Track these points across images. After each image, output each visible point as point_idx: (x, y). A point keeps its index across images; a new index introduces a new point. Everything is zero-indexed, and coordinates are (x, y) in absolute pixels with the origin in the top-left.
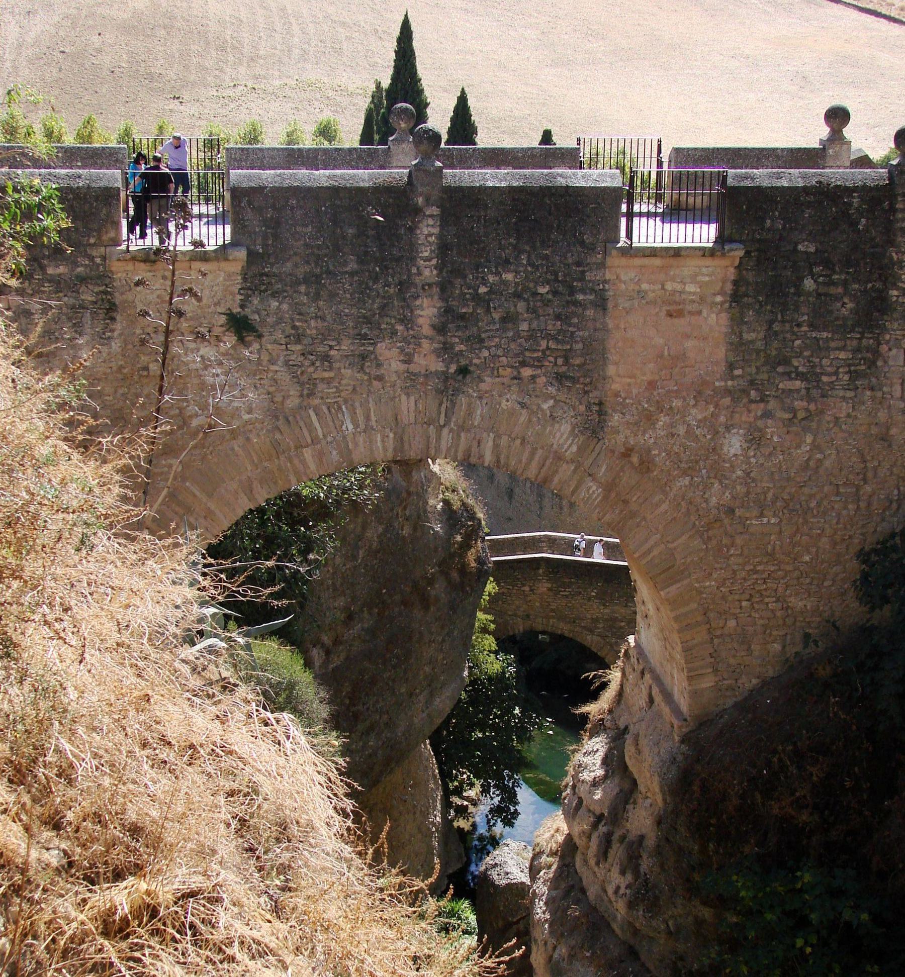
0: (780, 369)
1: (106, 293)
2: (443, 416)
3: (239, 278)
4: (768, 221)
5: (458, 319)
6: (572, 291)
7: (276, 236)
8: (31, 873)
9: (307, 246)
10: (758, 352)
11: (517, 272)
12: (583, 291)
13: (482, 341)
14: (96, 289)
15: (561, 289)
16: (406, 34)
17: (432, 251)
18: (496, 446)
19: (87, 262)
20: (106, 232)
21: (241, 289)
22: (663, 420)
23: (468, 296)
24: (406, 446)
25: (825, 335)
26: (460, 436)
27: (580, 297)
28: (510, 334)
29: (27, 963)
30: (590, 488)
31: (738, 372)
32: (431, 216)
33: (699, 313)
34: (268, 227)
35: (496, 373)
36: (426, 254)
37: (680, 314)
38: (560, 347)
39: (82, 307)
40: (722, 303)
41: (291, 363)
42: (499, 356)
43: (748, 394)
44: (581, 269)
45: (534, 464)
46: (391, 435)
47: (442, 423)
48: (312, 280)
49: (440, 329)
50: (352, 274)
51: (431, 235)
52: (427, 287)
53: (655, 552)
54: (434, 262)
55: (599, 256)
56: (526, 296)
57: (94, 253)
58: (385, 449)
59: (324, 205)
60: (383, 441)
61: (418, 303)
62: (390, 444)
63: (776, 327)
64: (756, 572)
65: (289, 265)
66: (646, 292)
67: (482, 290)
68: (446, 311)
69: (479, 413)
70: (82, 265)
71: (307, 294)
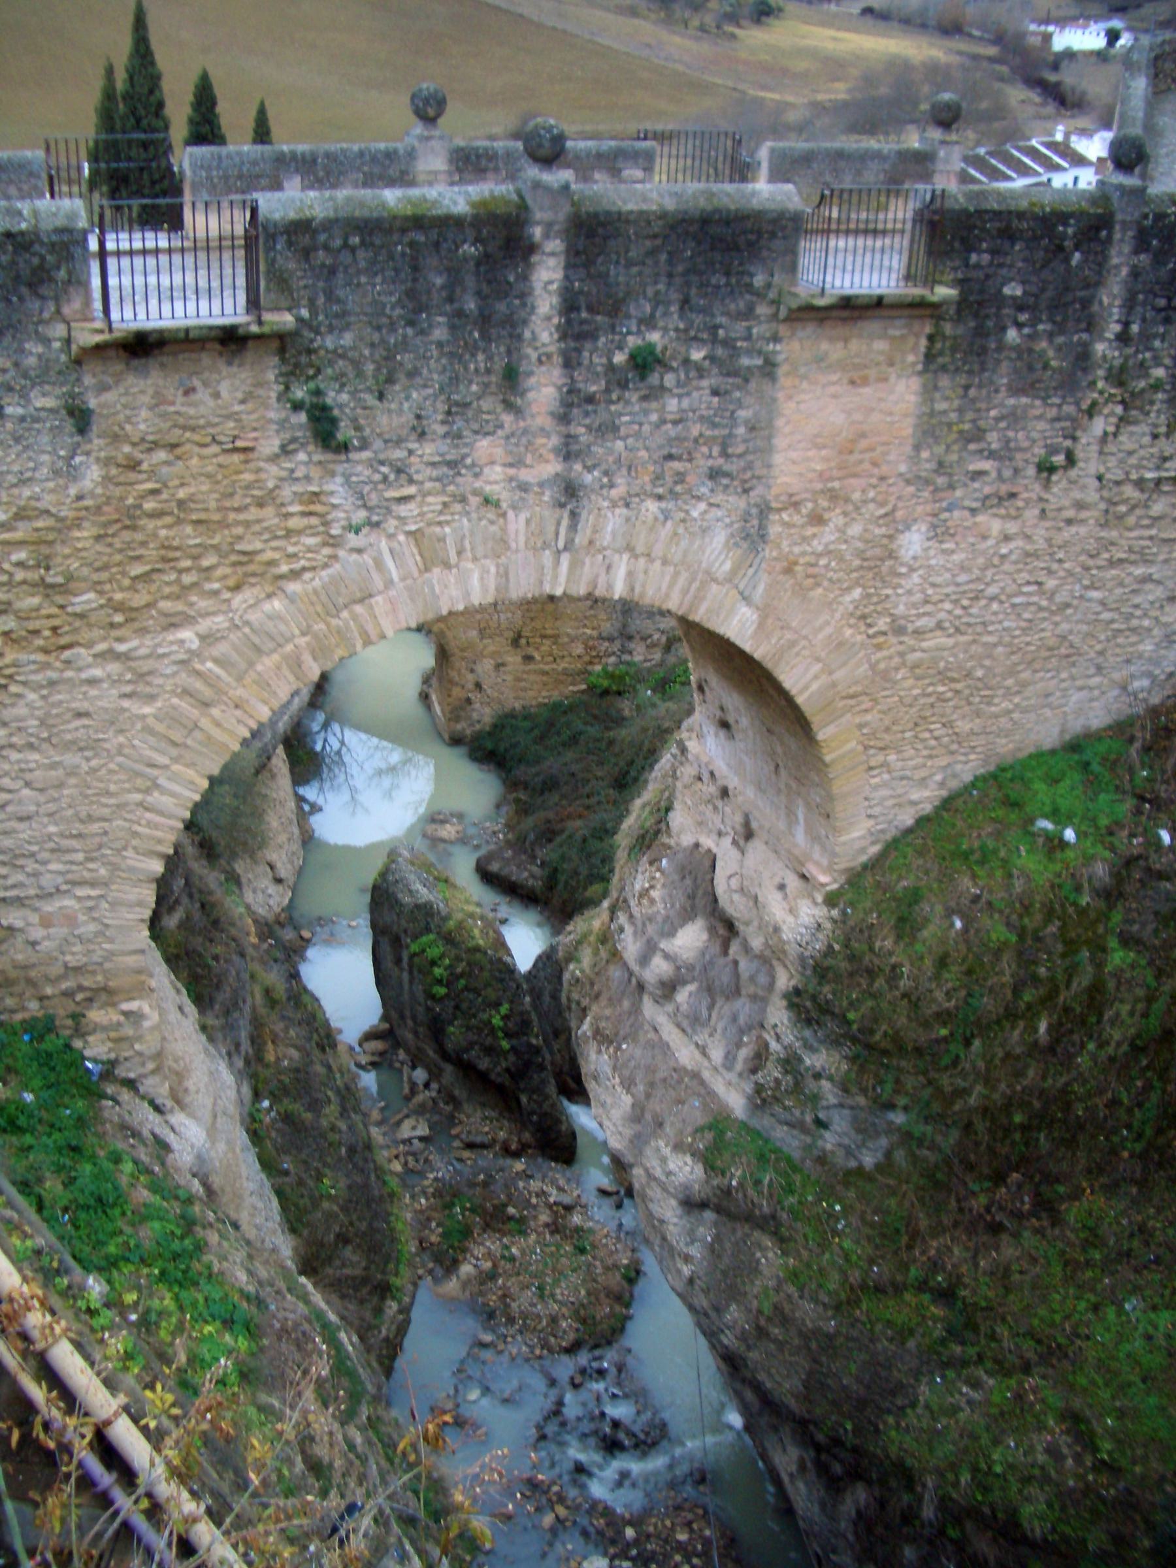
0: (972, 447)
8: (553, 1448)
12: (749, 352)
16: (140, 23)
18: (630, 574)
22: (836, 519)
28: (654, 417)
46: (493, 570)
47: (561, 544)
53: (815, 686)
58: (484, 589)
62: (492, 584)
63: (972, 392)
68: (570, 392)
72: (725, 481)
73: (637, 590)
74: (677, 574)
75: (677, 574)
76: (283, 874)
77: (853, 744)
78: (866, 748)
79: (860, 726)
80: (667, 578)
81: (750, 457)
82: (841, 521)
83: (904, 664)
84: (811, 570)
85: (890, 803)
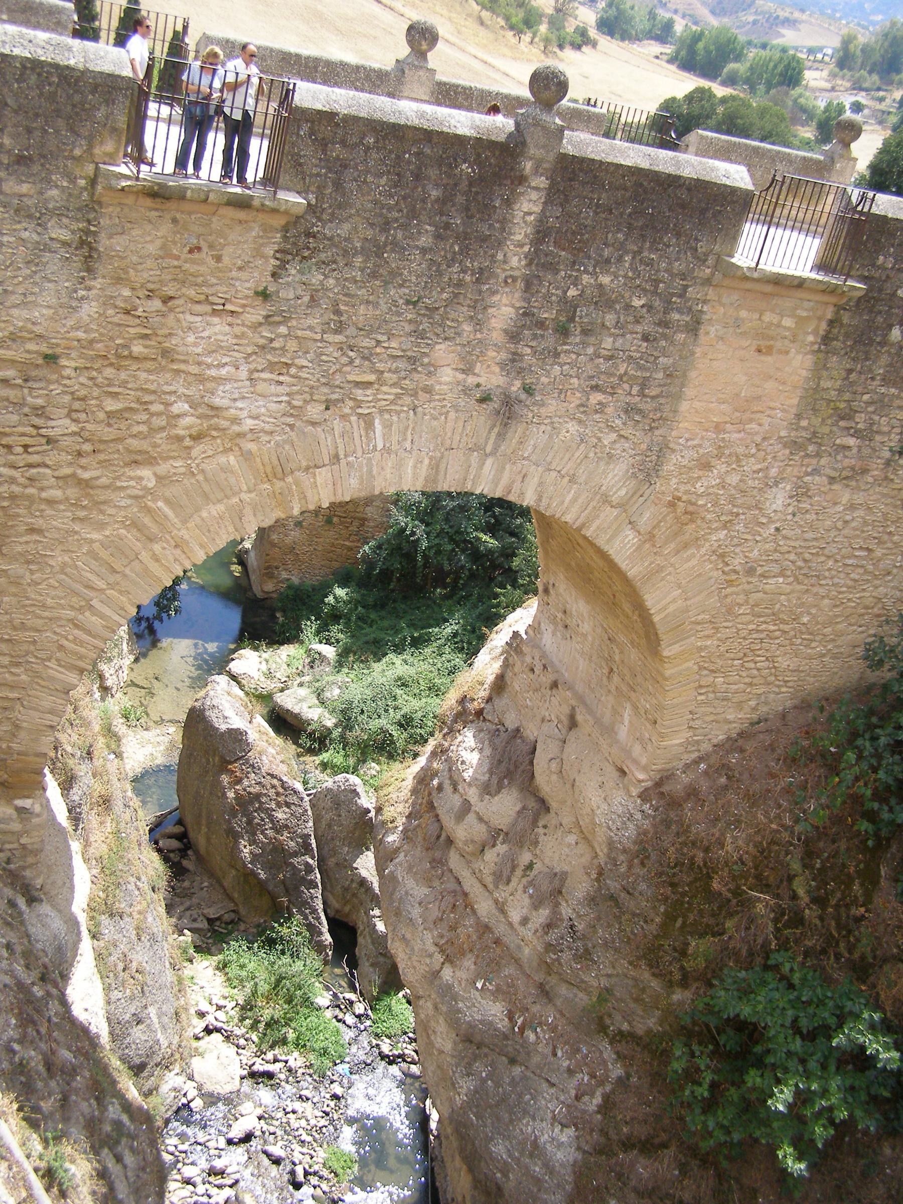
0: (842, 424)
1: (87, 232)
2: (491, 442)
3: (279, 235)
4: (881, 258)
5: (536, 325)
6: (668, 307)
7: (338, 185)
9: (376, 202)
10: (829, 401)
11: (616, 277)
13: (557, 355)
14: (74, 227)
15: (657, 303)
17: (526, 235)
19: (65, 184)
20: (102, 143)
21: (277, 251)
23: (554, 298)
24: (441, 477)
25: (893, 390)
26: (504, 468)
27: (676, 316)
29: (867, 594)
30: (627, 536)
31: (804, 423)
32: (536, 189)
33: (787, 353)
34: (330, 170)
35: (562, 396)
36: (519, 237)
37: (769, 351)
38: (639, 374)
39: (47, 249)
40: (813, 343)
41: (324, 358)
42: (571, 376)
43: (806, 449)
44: (685, 283)
45: (575, 510)
48: (376, 250)
49: (514, 336)
50: (424, 251)
51: (530, 214)
52: (509, 281)
53: (671, 608)
54: (526, 249)
55: (708, 271)
56: (618, 307)
57: (78, 172)
58: (415, 477)
59: (409, 152)
60: (415, 467)
61: (496, 298)
62: (423, 471)
64: (758, 631)
65: (347, 226)
66: (743, 320)
67: (572, 292)
68: (525, 314)
69: (532, 442)
70: (57, 186)
71: (362, 270)
72: (637, 418)
77: (690, 664)
79: (700, 649)
81: (662, 401)
82: (723, 468)
83: (747, 602)
84: (691, 508)
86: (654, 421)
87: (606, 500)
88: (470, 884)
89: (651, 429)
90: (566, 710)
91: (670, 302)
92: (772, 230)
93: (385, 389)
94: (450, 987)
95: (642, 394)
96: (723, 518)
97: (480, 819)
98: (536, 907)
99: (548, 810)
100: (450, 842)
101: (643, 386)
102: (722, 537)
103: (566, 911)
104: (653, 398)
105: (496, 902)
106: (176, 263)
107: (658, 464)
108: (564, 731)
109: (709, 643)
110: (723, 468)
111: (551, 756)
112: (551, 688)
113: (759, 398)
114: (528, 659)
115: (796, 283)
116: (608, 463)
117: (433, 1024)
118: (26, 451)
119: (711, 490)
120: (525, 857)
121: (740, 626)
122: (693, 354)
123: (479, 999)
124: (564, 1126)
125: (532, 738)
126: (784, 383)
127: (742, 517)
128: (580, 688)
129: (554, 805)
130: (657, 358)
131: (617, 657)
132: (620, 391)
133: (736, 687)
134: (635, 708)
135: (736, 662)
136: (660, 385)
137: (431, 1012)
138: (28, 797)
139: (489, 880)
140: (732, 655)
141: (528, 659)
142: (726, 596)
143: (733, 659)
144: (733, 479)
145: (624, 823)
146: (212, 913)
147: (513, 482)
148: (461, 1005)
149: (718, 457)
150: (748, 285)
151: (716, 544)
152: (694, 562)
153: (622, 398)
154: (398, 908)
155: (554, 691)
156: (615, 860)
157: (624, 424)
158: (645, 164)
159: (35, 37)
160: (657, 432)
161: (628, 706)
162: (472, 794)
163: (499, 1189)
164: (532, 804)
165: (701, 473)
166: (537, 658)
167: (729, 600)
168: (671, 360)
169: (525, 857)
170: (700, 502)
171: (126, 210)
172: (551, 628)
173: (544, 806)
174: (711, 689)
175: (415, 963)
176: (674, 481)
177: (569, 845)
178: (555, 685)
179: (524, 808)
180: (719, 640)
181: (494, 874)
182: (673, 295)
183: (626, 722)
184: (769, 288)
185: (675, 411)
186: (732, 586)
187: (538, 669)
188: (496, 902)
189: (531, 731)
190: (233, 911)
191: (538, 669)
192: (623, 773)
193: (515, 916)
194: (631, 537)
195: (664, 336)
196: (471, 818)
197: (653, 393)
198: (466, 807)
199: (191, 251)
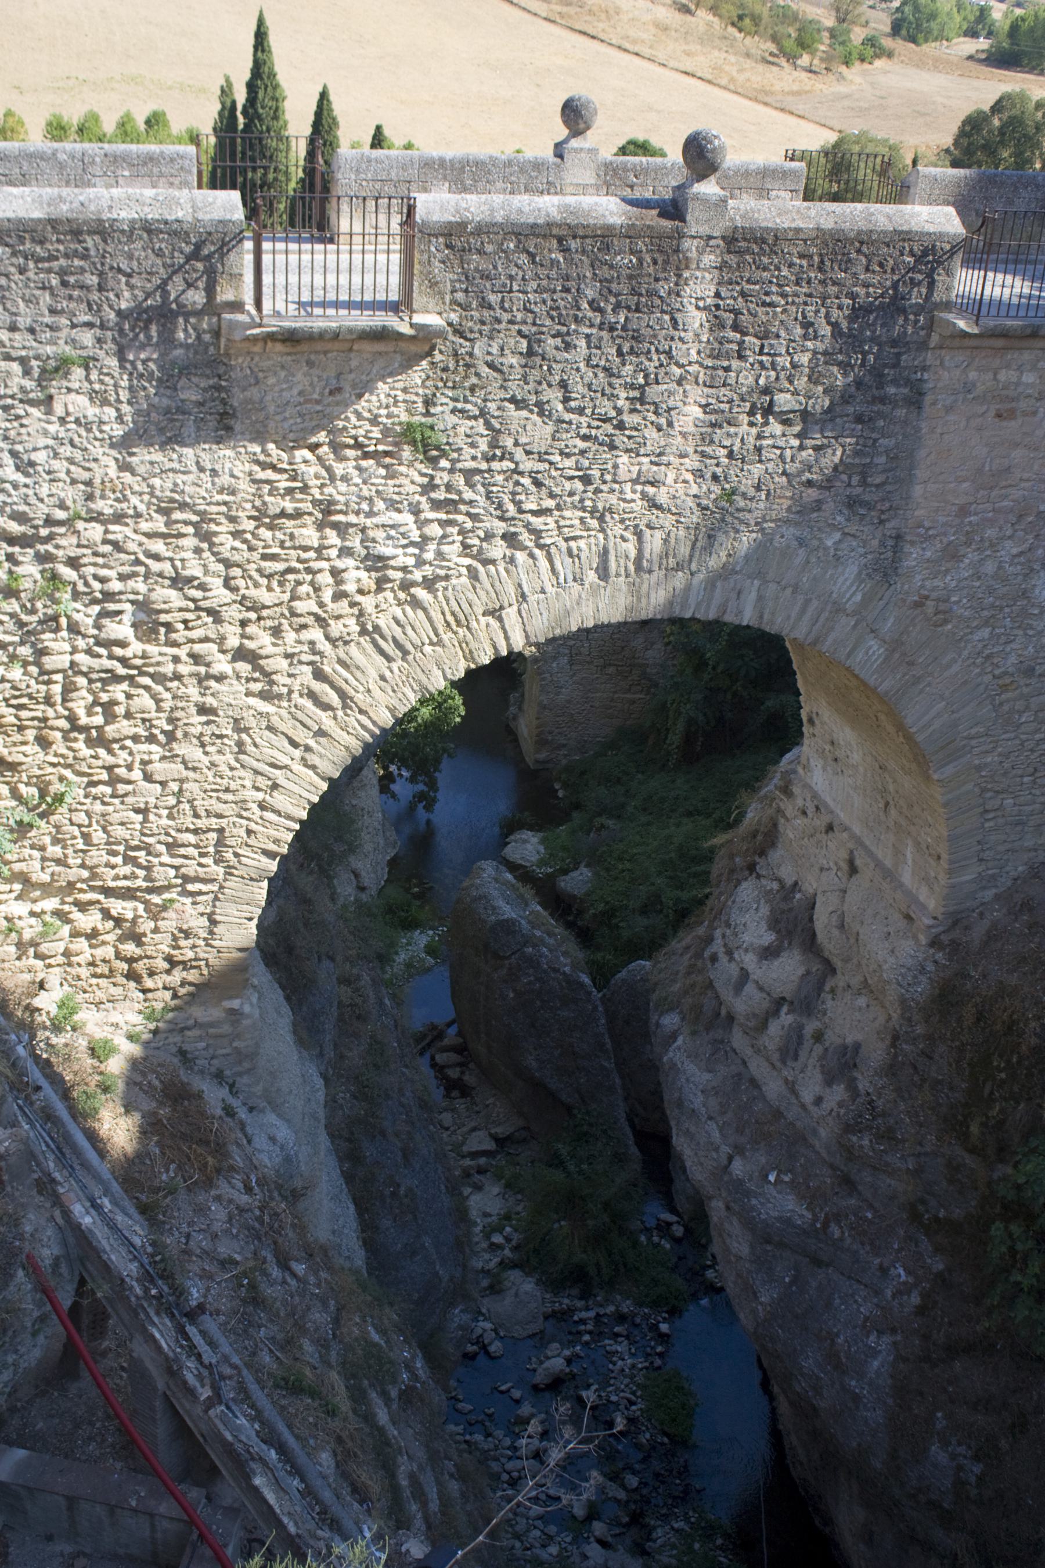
1: (218, 388)
27: (892, 390)
30: (870, 647)
37: (1011, 414)
72: (862, 511)
73: (765, 620)
74: (807, 602)
75: (807, 602)
76: (366, 882)
77: (969, 786)
78: (984, 790)
79: (979, 768)
80: (797, 609)
81: (889, 488)
82: (975, 557)
83: (1027, 708)
84: (942, 607)
85: (1001, 848)
86: (883, 512)
87: (838, 609)
88: (758, 1068)
89: (882, 522)
90: (844, 855)
91: (881, 375)
92: (990, 275)
93: (567, 514)
94: (740, 1182)
95: (864, 483)
96: (985, 613)
97: (761, 989)
98: (829, 1082)
99: (834, 971)
100: (731, 1018)
101: (864, 476)
102: (987, 636)
103: (863, 1085)
104: (877, 486)
105: (786, 1081)
106: (319, 408)
107: (896, 560)
108: (844, 880)
109: (989, 759)
110: (975, 557)
111: (831, 909)
112: (827, 832)
113: (1008, 469)
114: (800, 802)
115: (1029, 331)
116: (836, 567)
117: (727, 1225)
118: (187, 628)
119: (962, 584)
120: (811, 1027)
121: (1023, 737)
122: (918, 430)
123: (775, 1193)
124: (880, 1333)
125: (811, 891)
126: (1036, 449)
127: (1007, 610)
128: (857, 829)
129: (838, 963)
130: (875, 441)
131: (891, 787)
132: (838, 484)
133: (1030, 808)
134: (917, 844)
135: (1026, 779)
136: (884, 471)
137: (723, 1213)
138: (236, 997)
139: (776, 1057)
140: (1020, 772)
141: (800, 802)
142: (1001, 704)
143: (1022, 776)
144: (990, 568)
145: (915, 977)
146: (499, 1130)
147: (727, 600)
148: (754, 1202)
149: (968, 544)
150: (967, 342)
151: (980, 645)
152: (955, 668)
153: (841, 491)
154: (680, 1099)
155: (831, 835)
156: (909, 1020)
157: (848, 520)
158: (828, 224)
159: (141, 195)
160: (888, 525)
161: (910, 842)
162: (749, 960)
163: (815, 1409)
164: (816, 967)
165: (949, 565)
166: (808, 799)
167: (1006, 708)
168: (893, 441)
169: (811, 1027)
170: (953, 599)
171: (257, 359)
172: (820, 763)
173: (830, 969)
174: (999, 813)
175: (702, 1159)
176: (918, 577)
177: (860, 1009)
178: (830, 828)
179: (808, 973)
180: (1000, 755)
181: (780, 1049)
182: (885, 366)
183: (910, 862)
184: (1000, 343)
185: (909, 497)
186: (1007, 691)
187: (810, 811)
188: (786, 1081)
189: (811, 884)
190: (524, 1128)
191: (810, 811)
192: (908, 918)
193: (807, 1096)
194: (875, 648)
195: (881, 415)
196: (749, 988)
197: (878, 481)
198: (744, 975)
199: (331, 393)
